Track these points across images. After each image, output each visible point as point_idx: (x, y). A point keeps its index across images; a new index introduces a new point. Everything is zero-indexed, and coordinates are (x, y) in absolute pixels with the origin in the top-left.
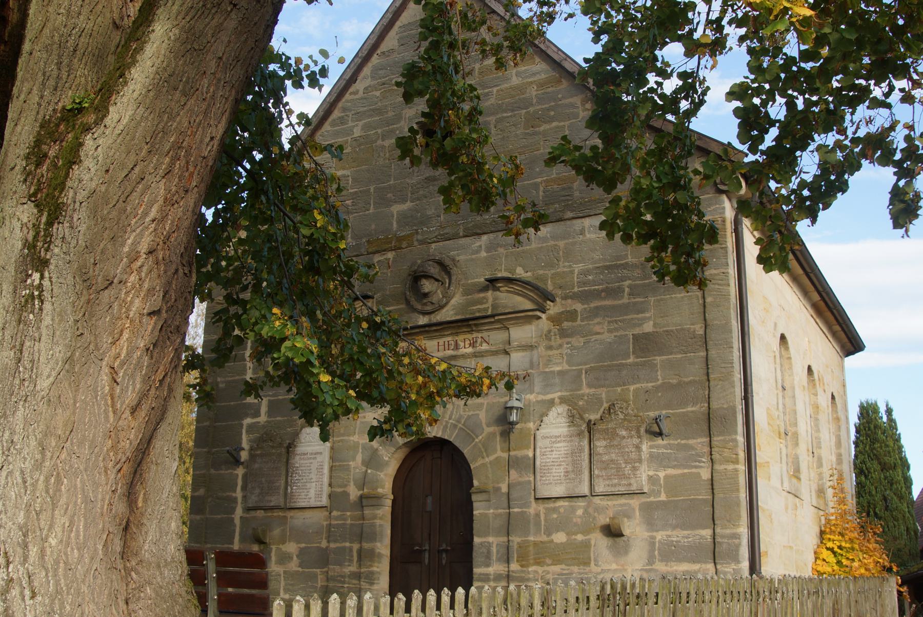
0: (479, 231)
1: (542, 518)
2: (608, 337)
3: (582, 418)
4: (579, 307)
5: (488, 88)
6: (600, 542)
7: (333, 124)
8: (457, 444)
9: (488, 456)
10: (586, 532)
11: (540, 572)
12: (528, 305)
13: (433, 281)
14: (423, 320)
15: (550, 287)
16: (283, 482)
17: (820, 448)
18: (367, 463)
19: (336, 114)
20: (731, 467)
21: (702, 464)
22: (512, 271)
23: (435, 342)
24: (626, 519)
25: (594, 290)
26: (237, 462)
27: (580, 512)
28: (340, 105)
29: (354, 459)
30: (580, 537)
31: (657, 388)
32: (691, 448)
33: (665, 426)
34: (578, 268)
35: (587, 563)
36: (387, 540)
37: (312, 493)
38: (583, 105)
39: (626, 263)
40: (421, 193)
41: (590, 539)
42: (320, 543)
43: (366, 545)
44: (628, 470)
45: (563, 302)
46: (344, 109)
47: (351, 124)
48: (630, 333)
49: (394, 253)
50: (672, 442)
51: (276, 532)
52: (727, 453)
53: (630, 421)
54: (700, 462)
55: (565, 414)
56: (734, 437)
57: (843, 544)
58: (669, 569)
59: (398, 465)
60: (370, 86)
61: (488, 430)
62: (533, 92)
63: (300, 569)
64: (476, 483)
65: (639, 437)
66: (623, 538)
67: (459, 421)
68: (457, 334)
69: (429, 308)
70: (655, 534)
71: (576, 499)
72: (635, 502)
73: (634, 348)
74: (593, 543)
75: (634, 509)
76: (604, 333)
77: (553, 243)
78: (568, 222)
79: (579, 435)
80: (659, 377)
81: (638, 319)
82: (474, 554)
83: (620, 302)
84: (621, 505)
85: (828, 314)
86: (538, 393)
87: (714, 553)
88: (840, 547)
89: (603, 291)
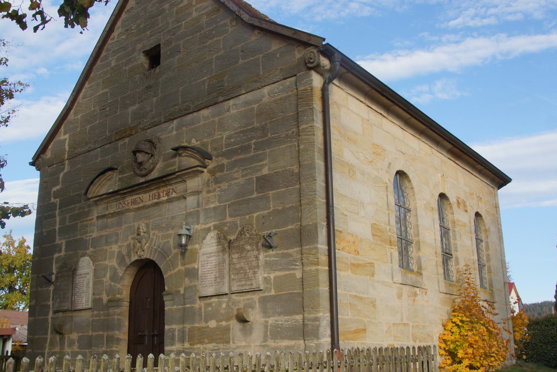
0: (172, 118)
1: (203, 311)
2: (241, 181)
3: (225, 238)
4: (225, 161)
5: (180, 22)
6: (235, 325)
7: (101, 62)
8: (157, 262)
9: (174, 270)
10: (228, 320)
11: (202, 348)
12: (197, 163)
13: (144, 154)
14: (142, 180)
15: (209, 150)
16: (70, 293)
17: (457, 251)
18: (112, 279)
19: (104, 54)
20: (314, 268)
21: (297, 267)
22: (190, 142)
23: (147, 195)
24: (250, 310)
25: (235, 148)
26: (50, 282)
27: (224, 305)
28: (105, 48)
29: (105, 276)
30: (224, 323)
31: (270, 214)
32: (290, 255)
33: (274, 241)
34: (225, 134)
35: (228, 342)
36: (126, 329)
37: (84, 300)
38: (231, 23)
39: (253, 128)
40: (143, 97)
41: (230, 324)
42: (88, 332)
43: (110, 333)
44: (250, 275)
45: (217, 159)
46: (108, 50)
47: (110, 59)
48: (254, 177)
49: (129, 138)
50: (278, 252)
51: (68, 327)
52: (311, 258)
53: (253, 239)
54: (296, 265)
55: (215, 237)
56: (316, 245)
57: (464, 319)
58: (276, 345)
59: (132, 280)
60: (120, 33)
61: (174, 251)
62: (204, 19)
63: (79, 350)
64: (166, 288)
65: (258, 250)
66: (249, 323)
67: (159, 247)
68: (159, 188)
69: (144, 172)
70: (267, 319)
71: (221, 297)
72: (256, 297)
73: (256, 186)
74: (231, 327)
75: (255, 302)
76: (239, 178)
77: (212, 119)
78: (221, 104)
79: (223, 251)
80: (271, 206)
81: (259, 166)
82: (165, 337)
83: (249, 155)
84: (248, 299)
85: (466, 157)
86: (202, 224)
87: (306, 332)
88: (462, 321)
89: (239, 148)
